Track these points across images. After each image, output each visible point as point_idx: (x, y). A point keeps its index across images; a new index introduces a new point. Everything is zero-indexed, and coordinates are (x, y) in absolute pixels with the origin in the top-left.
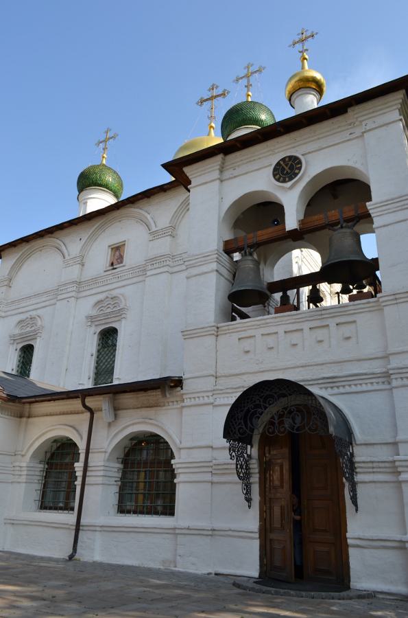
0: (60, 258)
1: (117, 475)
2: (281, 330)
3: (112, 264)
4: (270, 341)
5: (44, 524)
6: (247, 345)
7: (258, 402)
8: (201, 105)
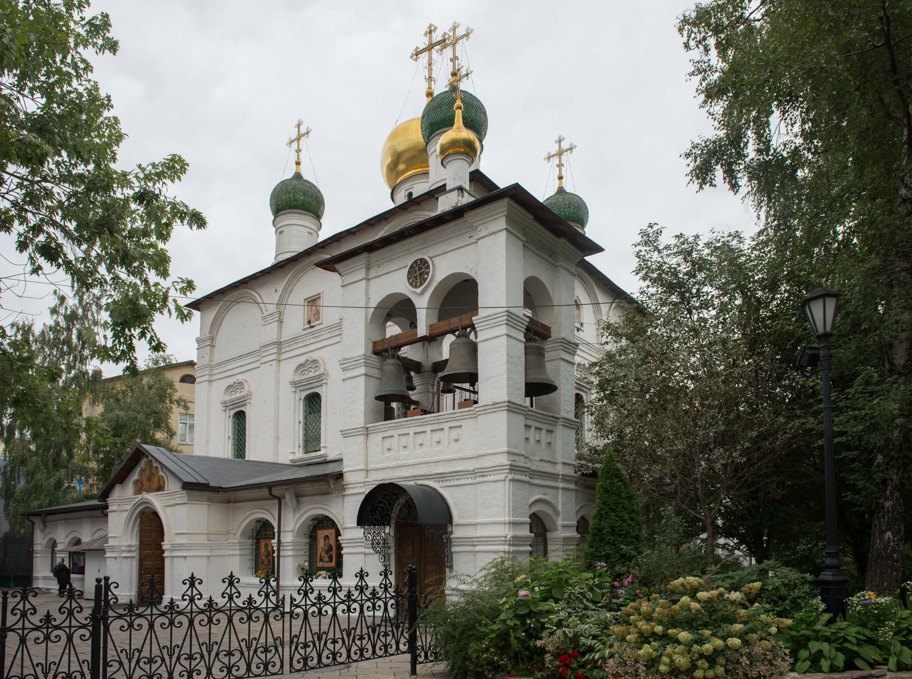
0: (258, 311)
1: (305, 547)
2: (411, 431)
3: (309, 322)
4: (404, 440)
5: (521, 469)
6: (388, 443)
7: (379, 499)
8: (416, 60)
